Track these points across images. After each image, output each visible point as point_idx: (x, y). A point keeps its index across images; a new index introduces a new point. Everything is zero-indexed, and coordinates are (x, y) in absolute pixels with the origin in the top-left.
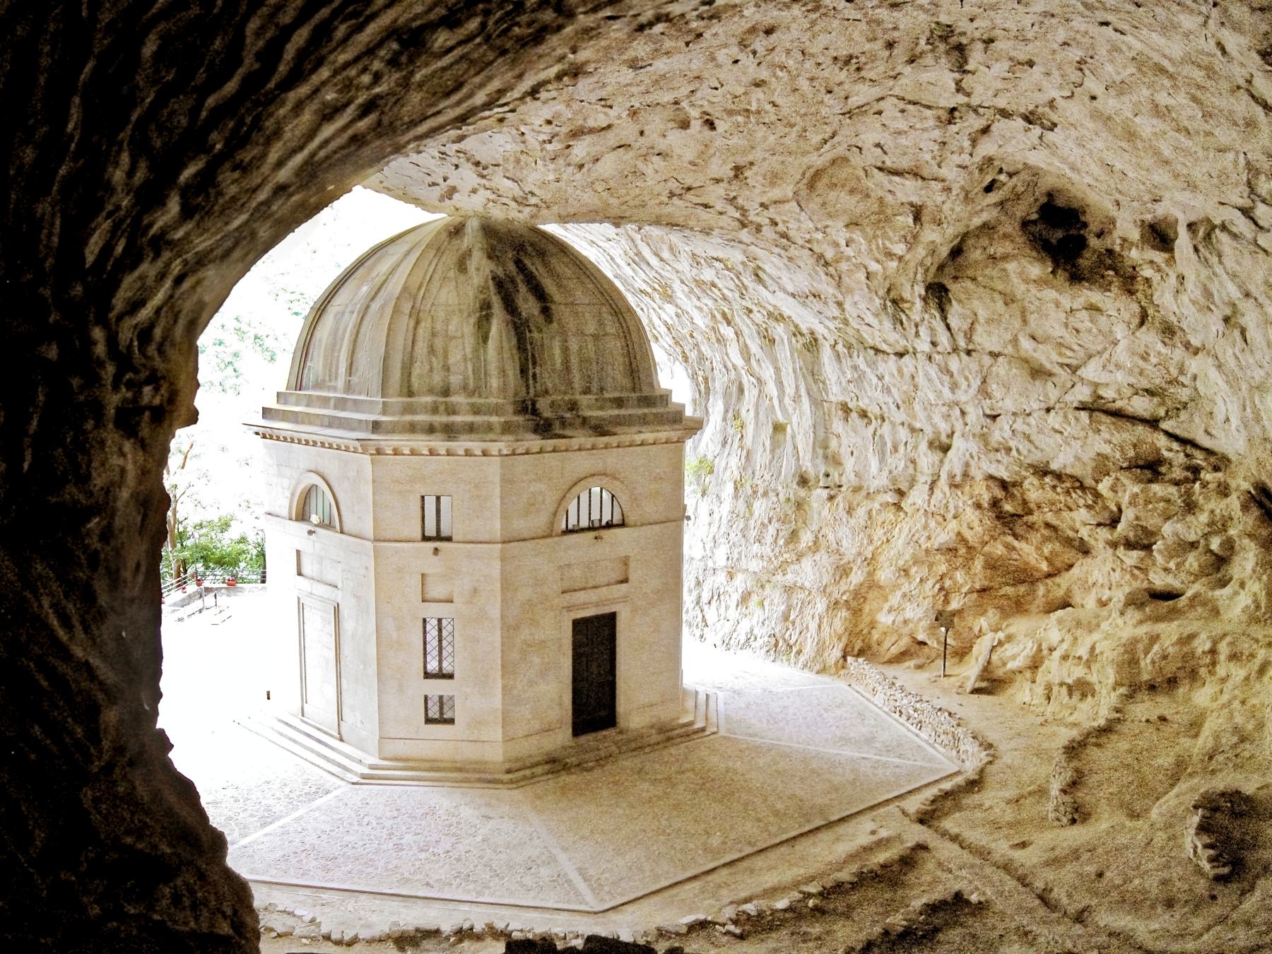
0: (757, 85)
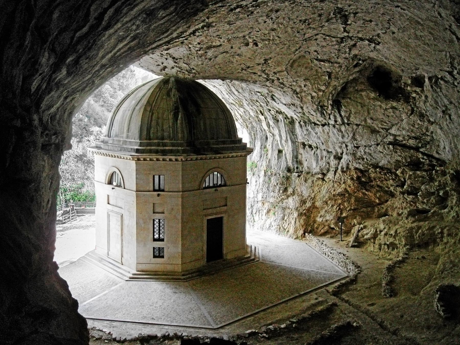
0: (273, 30)
